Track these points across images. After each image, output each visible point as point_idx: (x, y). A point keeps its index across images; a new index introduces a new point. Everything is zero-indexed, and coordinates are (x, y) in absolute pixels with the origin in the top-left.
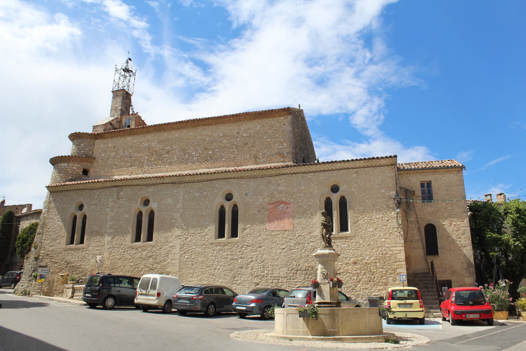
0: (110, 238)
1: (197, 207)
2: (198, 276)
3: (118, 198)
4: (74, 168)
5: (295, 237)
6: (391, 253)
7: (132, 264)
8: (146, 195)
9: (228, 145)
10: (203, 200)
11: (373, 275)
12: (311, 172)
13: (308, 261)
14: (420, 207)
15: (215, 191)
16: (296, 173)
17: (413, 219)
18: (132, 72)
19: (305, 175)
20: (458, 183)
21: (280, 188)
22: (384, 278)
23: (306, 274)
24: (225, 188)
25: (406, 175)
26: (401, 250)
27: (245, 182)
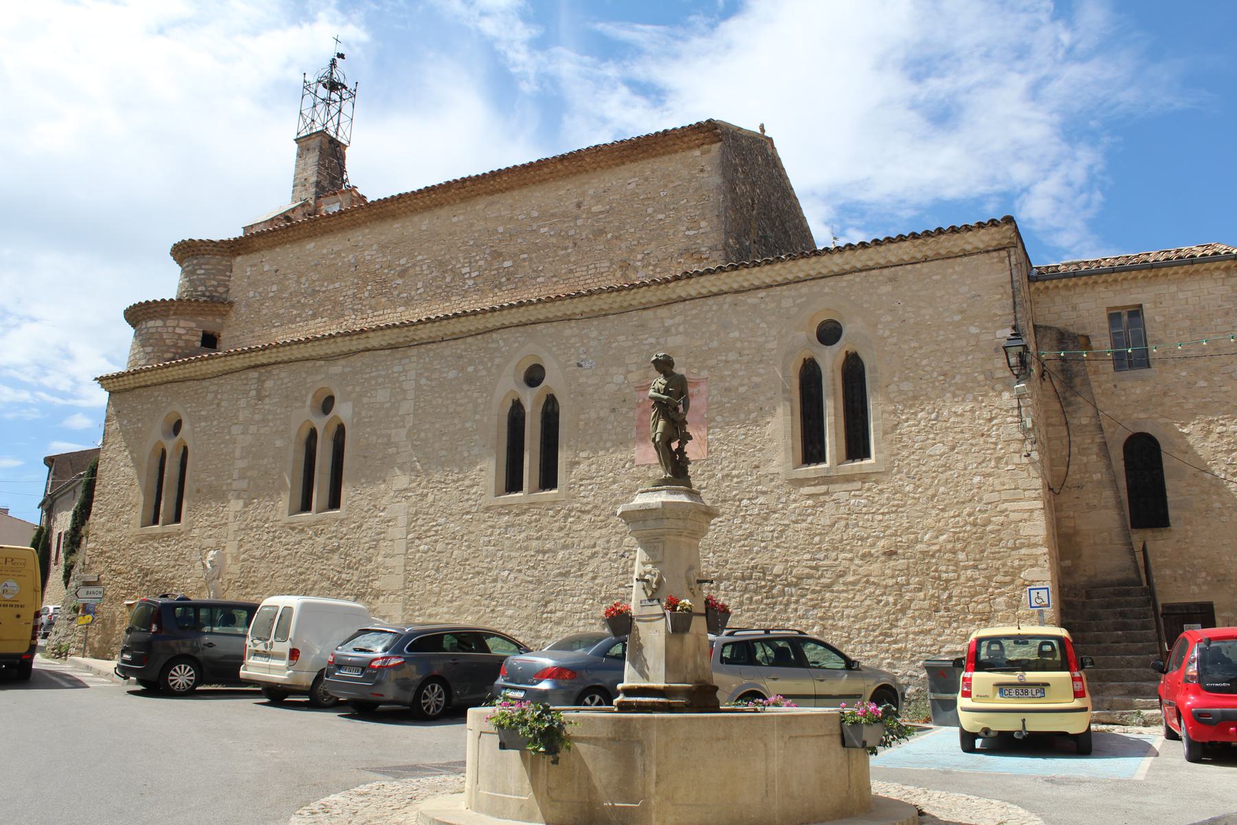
0: (241, 503)
1: (451, 410)
2: (451, 601)
3: (260, 398)
4: (178, 330)
5: (713, 481)
6: (1001, 519)
7: (290, 571)
8: (319, 386)
9: (553, 240)
10: (465, 387)
11: (945, 589)
12: (758, 288)
13: (751, 551)
15: (497, 361)
17: (1085, 421)
19: (740, 297)
20: (1227, 306)
22: (981, 598)
23: (745, 590)
24: (519, 350)
25: (1063, 292)
26: (1032, 511)
27: (576, 331)
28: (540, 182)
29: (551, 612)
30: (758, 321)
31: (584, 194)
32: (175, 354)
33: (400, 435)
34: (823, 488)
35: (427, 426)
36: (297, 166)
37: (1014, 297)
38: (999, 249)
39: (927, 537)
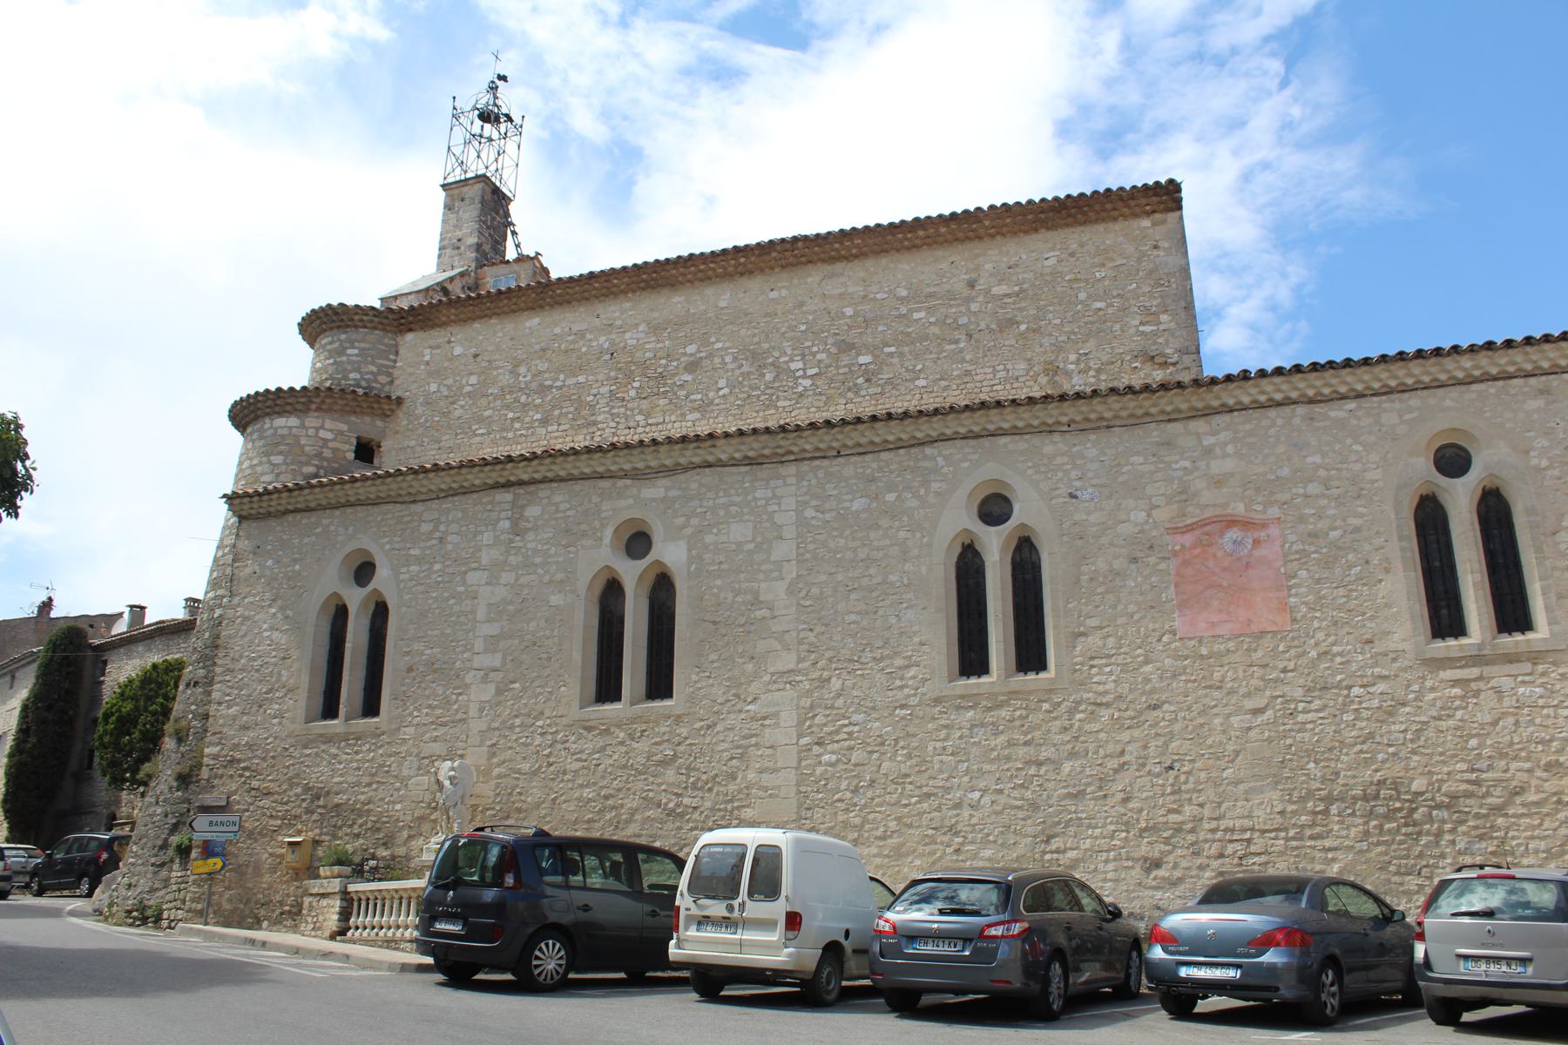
1: (863, 556)
4: (322, 434)
5: (1303, 661)
9: (936, 330)
10: (884, 523)
12: (1343, 397)
13: (1373, 759)
16: (1279, 404)
18: (509, 119)
21: (1218, 466)
23: (1370, 814)
28: (908, 249)
29: (1057, 851)
30: (1349, 441)
31: (977, 269)
32: (319, 468)
33: (776, 592)
34: (1474, 672)
35: (823, 578)
36: (444, 221)
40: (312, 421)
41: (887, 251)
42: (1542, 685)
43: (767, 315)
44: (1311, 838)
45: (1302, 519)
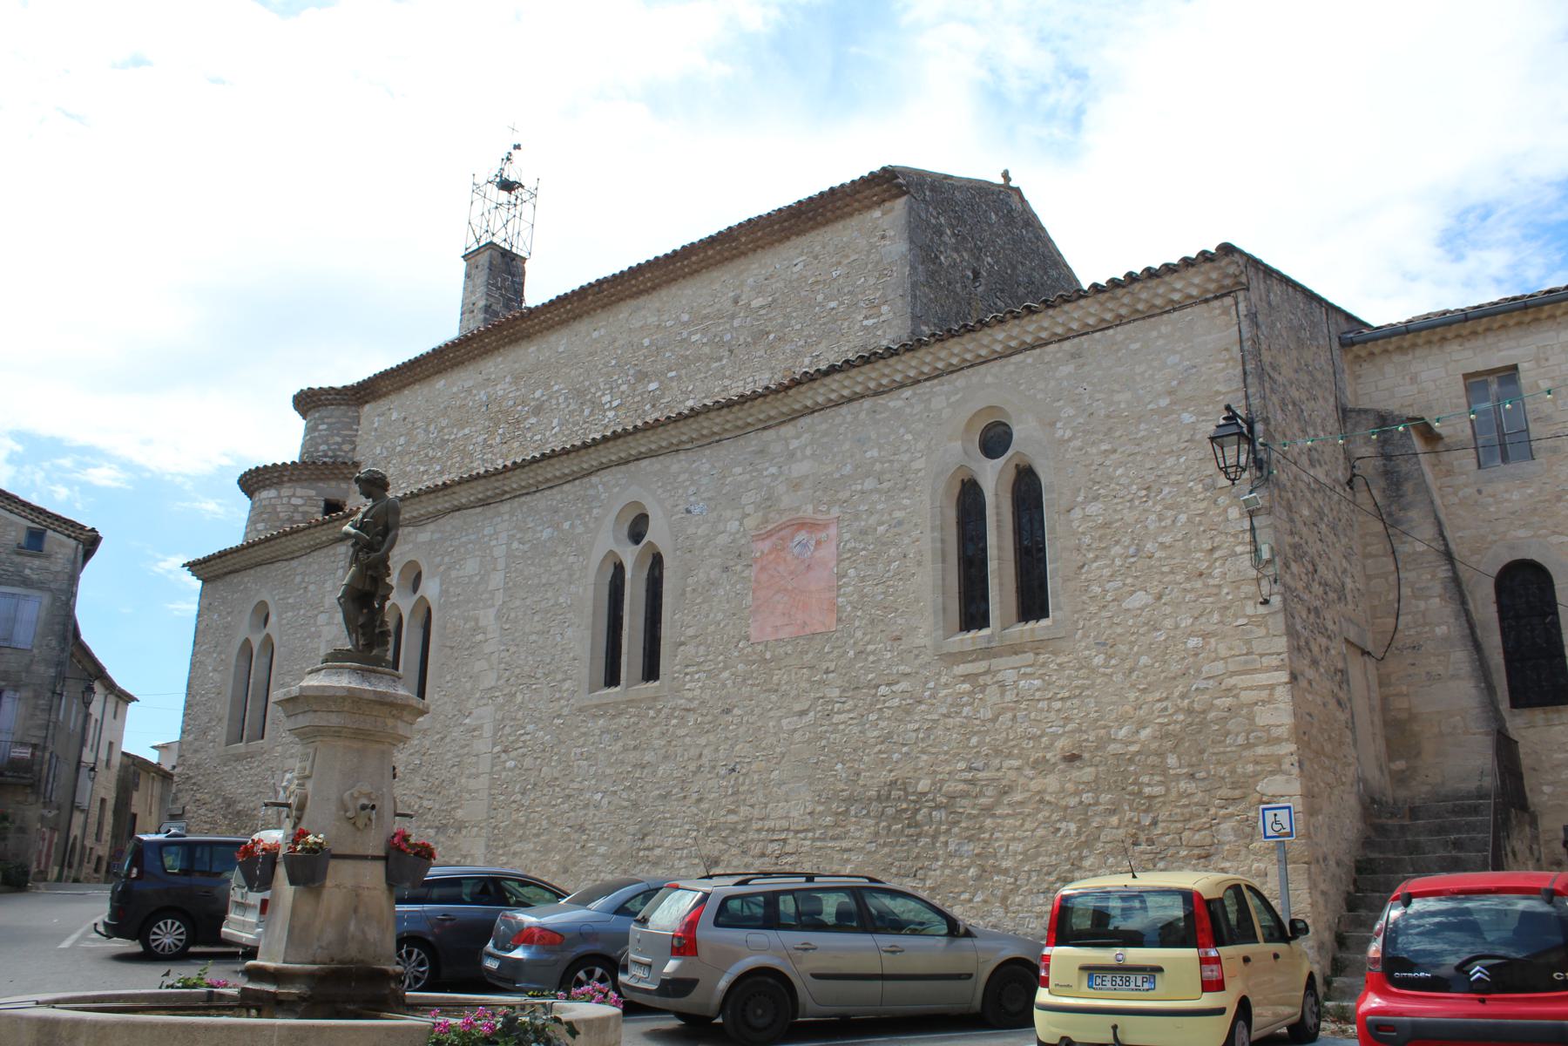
2: (537, 835)
4: (294, 501)
6: (1228, 701)
9: (707, 350)
12: (902, 386)
14: (1471, 491)
16: (850, 400)
19: (881, 400)
21: (801, 468)
25: (1397, 358)
26: (1272, 687)
29: (647, 849)
33: (488, 618)
34: (981, 666)
35: (518, 603)
37: (1244, 364)
38: (1223, 296)
39: (1123, 732)
40: (286, 491)
41: (675, 280)
42: (1041, 677)
43: (591, 354)
44: (833, 839)
45: (857, 517)
